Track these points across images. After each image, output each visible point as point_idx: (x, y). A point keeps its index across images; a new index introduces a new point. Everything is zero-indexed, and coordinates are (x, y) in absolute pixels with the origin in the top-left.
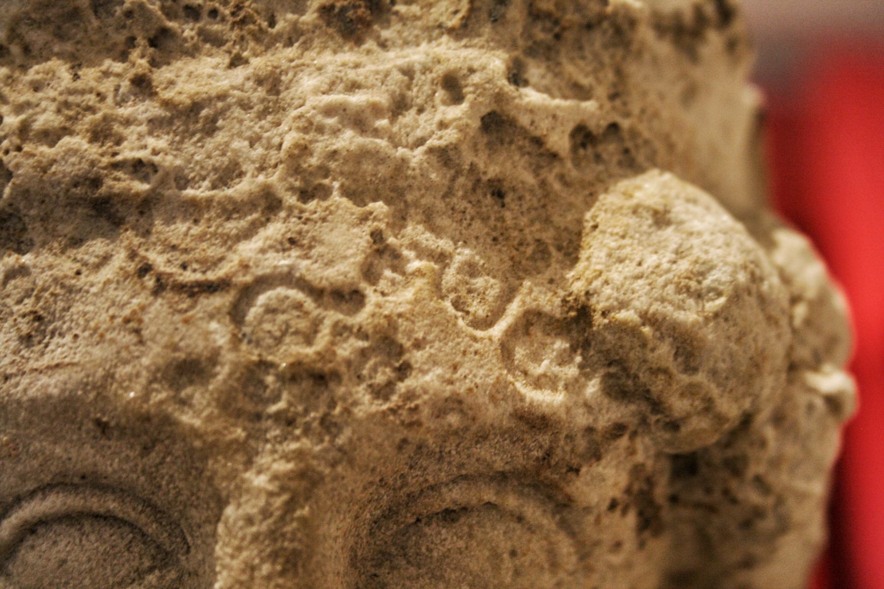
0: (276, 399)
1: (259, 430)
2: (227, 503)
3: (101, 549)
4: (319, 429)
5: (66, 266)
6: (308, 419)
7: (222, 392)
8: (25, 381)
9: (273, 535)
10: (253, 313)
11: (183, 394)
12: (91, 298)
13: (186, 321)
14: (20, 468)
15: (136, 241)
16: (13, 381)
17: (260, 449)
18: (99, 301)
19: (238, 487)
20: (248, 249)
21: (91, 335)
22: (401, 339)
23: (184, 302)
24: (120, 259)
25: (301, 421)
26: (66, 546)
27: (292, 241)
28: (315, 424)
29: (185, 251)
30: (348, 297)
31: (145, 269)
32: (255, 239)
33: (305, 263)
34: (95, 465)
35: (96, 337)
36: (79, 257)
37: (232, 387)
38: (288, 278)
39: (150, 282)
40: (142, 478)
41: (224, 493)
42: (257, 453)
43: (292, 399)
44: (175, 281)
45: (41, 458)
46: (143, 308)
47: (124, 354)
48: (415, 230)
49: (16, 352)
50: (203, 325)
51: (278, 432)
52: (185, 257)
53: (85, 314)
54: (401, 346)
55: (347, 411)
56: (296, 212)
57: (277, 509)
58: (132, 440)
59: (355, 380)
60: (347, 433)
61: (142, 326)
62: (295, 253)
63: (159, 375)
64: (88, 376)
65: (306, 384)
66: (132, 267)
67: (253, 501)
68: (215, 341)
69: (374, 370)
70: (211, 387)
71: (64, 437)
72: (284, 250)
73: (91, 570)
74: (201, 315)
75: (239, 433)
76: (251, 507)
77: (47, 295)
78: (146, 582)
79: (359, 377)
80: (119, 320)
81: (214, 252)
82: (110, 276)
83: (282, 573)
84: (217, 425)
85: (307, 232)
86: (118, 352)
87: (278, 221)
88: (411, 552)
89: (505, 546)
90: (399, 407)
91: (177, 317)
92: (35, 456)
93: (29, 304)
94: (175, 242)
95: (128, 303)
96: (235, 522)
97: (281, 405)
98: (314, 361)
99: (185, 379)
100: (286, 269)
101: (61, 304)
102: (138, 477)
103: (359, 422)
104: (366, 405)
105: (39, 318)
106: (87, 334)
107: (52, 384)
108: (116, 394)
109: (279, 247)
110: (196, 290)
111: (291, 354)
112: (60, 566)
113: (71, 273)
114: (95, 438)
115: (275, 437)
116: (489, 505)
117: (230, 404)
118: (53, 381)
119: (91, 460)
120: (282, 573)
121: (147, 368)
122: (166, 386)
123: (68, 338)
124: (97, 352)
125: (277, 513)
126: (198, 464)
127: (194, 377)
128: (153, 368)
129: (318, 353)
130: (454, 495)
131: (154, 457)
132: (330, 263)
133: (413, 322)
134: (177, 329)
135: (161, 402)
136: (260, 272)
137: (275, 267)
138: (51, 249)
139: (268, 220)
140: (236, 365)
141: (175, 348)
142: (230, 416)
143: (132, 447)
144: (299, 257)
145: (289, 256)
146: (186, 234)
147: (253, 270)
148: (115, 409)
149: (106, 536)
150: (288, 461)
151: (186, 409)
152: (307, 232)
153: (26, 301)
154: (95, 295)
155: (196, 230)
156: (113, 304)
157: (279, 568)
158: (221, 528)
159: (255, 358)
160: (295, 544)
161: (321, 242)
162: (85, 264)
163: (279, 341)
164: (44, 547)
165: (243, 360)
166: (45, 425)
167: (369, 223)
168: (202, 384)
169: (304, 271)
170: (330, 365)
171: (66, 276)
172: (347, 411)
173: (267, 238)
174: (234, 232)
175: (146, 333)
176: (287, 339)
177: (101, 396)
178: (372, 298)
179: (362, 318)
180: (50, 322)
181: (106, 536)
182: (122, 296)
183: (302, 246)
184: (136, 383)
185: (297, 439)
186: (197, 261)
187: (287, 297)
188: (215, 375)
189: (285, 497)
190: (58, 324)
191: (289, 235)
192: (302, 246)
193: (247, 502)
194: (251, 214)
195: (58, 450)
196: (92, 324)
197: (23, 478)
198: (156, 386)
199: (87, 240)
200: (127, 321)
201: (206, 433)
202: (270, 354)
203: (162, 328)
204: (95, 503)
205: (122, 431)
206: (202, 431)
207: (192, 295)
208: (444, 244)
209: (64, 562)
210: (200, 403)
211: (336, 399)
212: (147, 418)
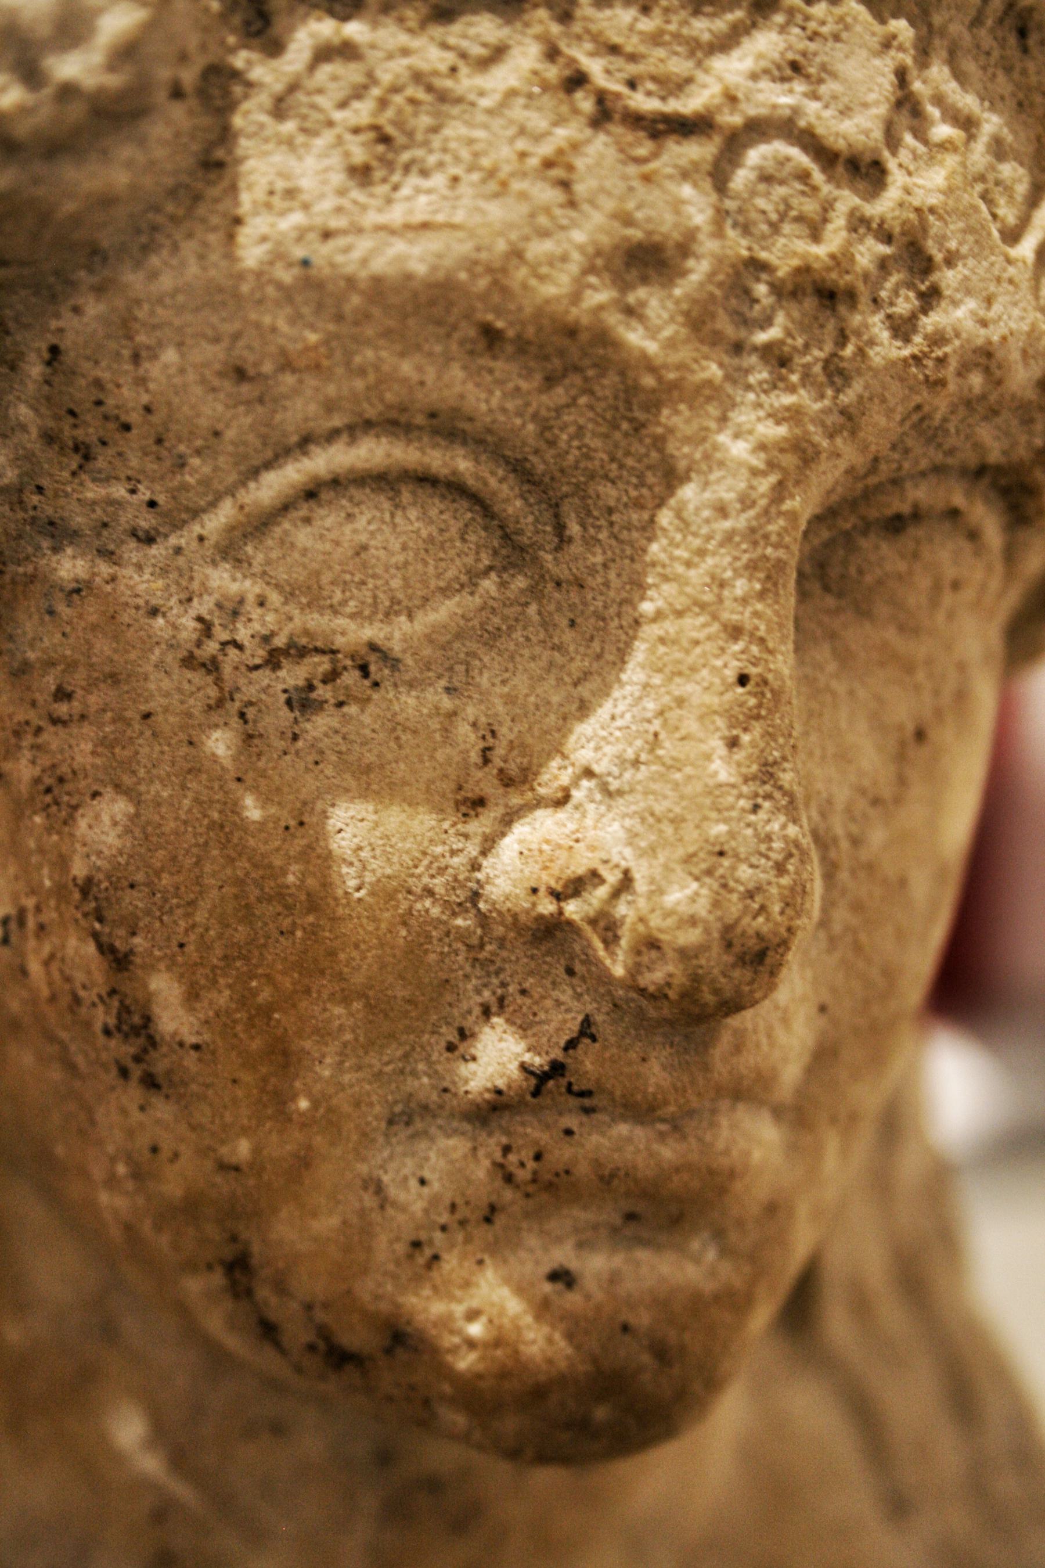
0: (766, 322)
1: (739, 369)
2: (686, 479)
3: (424, 533)
4: (822, 379)
5: (430, 54)
6: (808, 359)
7: (695, 301)
8: (363, 245)
9: (754, 535)
10: (741, 178)
11: (631, 299)
12: (481, 118)
13: (647, 178)
14: (331, 390)
15: (555, 29)
16: (341, 242)
17: (738, 399)
18: (497, 123)
19: (707, 457)
20: (733, 67)
21: (484, 181)
22: (932, 248)
23: (641, 145)
24: (525, 58)
25: (800, 360)
26: (369, 523)
27: (795, 66)
28: (817, 369)
29: (633, 58)
30: (865, 171)
31: (577, 80)
32: (736, 53)
33: (813, 107)
34: (462, 397)
35: (493, 186)
36: (452, 41)
37: (712, 295)
38: (787, 127)
39: (586, 103)
40: (531, 427)
41: (682, 465)
42: (734, 405)
43: (790, 326)
44: (626, 107)
45: (372, 378)
46: (575, 147)
47: (543, 220)
48: (939, 72)
49: (341, 192)
50: (671, 186)
51: (765, 375)
52: (633, 69)
53: (471, 142)
54: (930, 259)
55: (861, 352)
56: (799, 19)
57: (763, 496)
58: (532, 364)
59: (872, 307)
60: (857, 387)
61: (574, 177)
62: (799, 86)
63: (599, 262)
64: (478, 249)
65: (810, 303)
66: (553, 73)
67: (729, 481)
68: (690, 218)
69: (896, 292)
70: (678, 292)
71: (418, 347)
72: (783, 79)
73: (406, 563)
74: (669, 170)
75: (713, 371)
76: (727, 489)
77: (398, 99)
78: (481, 590)
79: (875, 301)
80: (534, 162)
81: (679, 66)
82: (513, 82)
83: (761, 595)
84: (684, 354)
85: (815, 54)
86: (532, 215)
87: (770, 29)
88: (834, 572)
89: (950, 572)
90: (925, 355)
91: (632, 170)
92: (362, 372)
93: (362, 111)
94: (617, 40)
95: (548, 134)
96: (697, 509)
97: (773, 333)
98: (829, 269)
99: (634, 273)
100: (787, 112)
101: (425, 120)
102: (524, 425)
103: (875, 372)
104: (887, 349)
105: (385, 139)
106: (475, 177)
107: (417, 257)
108: (525, 286)
109: (776, 73)
110: (661, 127)
111: (795, 254)
112: (358, 554)
113: (443, 68)
114: (471, 353)
115: (760, 383)
116: (954, 514)
117: (704, 322)
118: (416, 250)
119: (458, 389)
120: (761, 595)
121: (581, 248)
122: (608, 281)
123: (438, 180)
124: (496, 211)
125: (763, 502)
126: (640, 415)
127: (651, 272)
128: (590, 250)
129: (833, 256)
130: (920, 493)
131: (560, 394)
132: (845, 112)
133: (946, 223)
134: (631, 189)
135: (601, 307)
136: (752, 112)
137: (775, 107)
138: (401, 20)
139: (754, 25)
140: (719, 260)
141: (628, 220)
142: (702, 341)
143: (528, 375)
144: (805, 95)
145: (791, 91)
146: (631, 28)
147: (743, 106)
148: (520, 309)
149: (433, 512)
150: (778, 423)
151: (634, 323)
152: (815, 54)
153: (356, 105)
154: (490, 112)
155: (647, 25)
156: (522, 131)
157: (758, 586)
158: (665, 518)
159: (745, 253)
160: (781, 553)
161: (834, 75)
162: (463, 55)
163: (775, 228)
164: (329, 522)
165: (729, 252)
166: (391, 323)
167: (893, 52)
168: (663, 286)
169: (812, 120)
170: (848, 278)
171: (436, 73)
172: (861, 352)
173: (760, 56)
174: (706, 37)
175: (580, 189)
176: (787, 228)
177: (499, 286)
178: (897, 178)
179: (885, 206)
180: (406, 147)
181: (433, 512)
182: (538, 121)
183: (808, 77)
184: (562, 270)
185: (792, 389)
186: (654, 79)
187: (788, 159)
188: (684, 273)
189: (773, 479)
190: (419, 153)
191: (790, 56)
192: (808, 77)
193: (718, 481)
194: (731, 11)
195: (406, 368)
196: (486, 162)
197: (330, 407)
198: (593, 279)
199: (462, 13)
200: (548, 164)
201: (665, 366)
202: (763, 248)
203: (608, 184)
204: (438, 459)
205: (522, 346)
206: (658, 362)
207: (655, 135)
208: (968, 101)
209: (365, 548)
210: (659, 317)
211: (848, 332)
212: (572, 332)
